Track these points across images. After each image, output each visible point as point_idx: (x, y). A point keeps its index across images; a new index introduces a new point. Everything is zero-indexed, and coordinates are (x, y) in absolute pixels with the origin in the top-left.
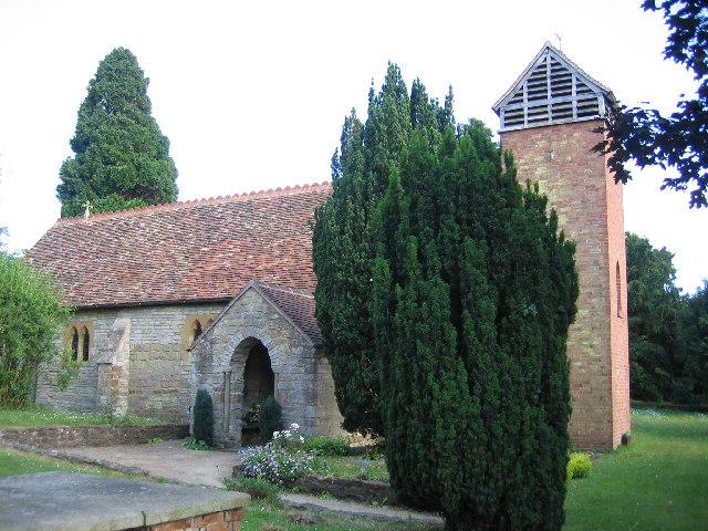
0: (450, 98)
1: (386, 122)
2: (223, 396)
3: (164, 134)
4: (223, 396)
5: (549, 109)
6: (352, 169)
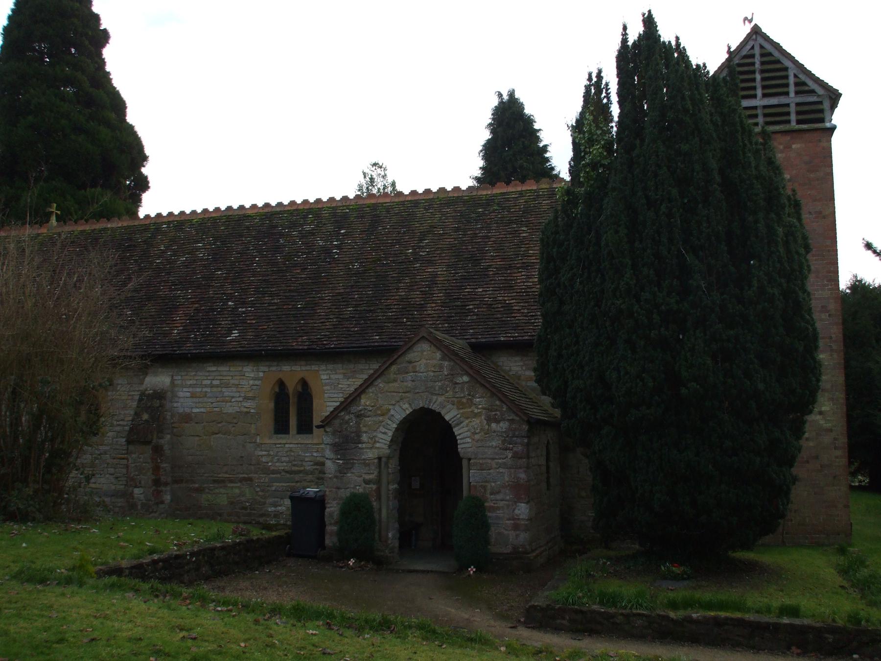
0: (677, 38)
1: (279, 609)
2: (378, 490)
3: (130, 123)
4: (378, 490)
5: (759, 112)
6: (293, 225)
